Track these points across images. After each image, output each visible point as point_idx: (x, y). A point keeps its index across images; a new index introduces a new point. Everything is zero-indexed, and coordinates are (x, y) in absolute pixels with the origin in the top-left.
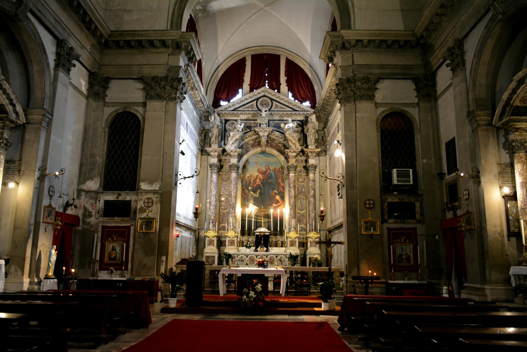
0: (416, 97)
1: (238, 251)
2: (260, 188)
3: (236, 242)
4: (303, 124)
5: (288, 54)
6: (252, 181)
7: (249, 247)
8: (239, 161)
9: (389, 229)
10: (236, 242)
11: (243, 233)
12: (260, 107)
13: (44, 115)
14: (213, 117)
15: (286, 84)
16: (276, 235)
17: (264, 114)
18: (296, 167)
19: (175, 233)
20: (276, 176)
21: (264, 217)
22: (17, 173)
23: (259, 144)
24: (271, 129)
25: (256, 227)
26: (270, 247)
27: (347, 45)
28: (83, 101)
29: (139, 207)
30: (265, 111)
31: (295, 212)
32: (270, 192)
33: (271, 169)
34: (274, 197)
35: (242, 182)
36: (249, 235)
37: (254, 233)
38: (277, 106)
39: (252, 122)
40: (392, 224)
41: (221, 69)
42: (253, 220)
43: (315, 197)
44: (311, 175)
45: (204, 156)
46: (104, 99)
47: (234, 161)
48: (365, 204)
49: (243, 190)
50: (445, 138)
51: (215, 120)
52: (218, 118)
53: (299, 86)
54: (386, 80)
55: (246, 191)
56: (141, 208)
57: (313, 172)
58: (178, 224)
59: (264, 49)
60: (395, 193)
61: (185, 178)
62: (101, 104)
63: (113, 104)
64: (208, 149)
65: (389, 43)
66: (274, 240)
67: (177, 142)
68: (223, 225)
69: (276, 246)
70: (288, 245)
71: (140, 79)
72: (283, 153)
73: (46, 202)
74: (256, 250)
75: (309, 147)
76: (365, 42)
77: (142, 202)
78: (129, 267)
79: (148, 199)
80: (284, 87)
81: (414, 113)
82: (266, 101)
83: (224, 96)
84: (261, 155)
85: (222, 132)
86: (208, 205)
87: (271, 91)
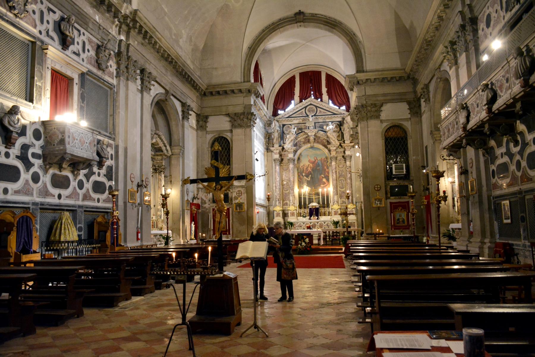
0: (409, 114)
1: (298, 220)
2: (311, 174)
3: (295, 213)
4: (340, 124)
5: (327, 70)
6: (305, 169)
7: (305, 217)
8: (294, 155)
9: (391, 203)
10: (295, 213)
11: (300, 207)
12: (308, 113)
13: (181, 150)
14: (273, 124)
15: (327, 94)
16: (324, 207)
17: (311, 119)
18: (336, 158)
19: (256, 211)
20: (322, 164)
21: (315, 195)
22: (169, 183)
23: (309, 141)
24: (316, 130)
25: (310, 203)
26: (320, 216)
27: (361, 82)
28: (195, 132)
29: (233, 196)
30: (312, 116)
31: (337, 191)
32: (319, 176)
33: (318, 159)
34: (322, 180)
35: (298, 170)
36: (305, 208)
37: (308, 207)
38: (320, 111)
39: (303, 125)
40: (393, 200)
41: (278, 85)
42: (307, 197)
43: (351, 179)
44: (348, 163)
45: (269, 153)
46: (206, 129)
47: (291, 156)
48: (375, 188)
49: (299, 176)
50: (425, 145)
51: (276, 126)
52: (277, 124)
53: (337, 94)
54: (388, 104)
55: (301, 176)
56: (235, 197)
57: (349, 160)
58: (257, 205)
59: (308, 68)
60: (395, 179)
61: (260, 176)
62: (205, 132)
63: (212, 132)
64: (272, 149)
65: (389, 79)
66: (323, 211)
67: (253, 154)
68: (285, 202)
69: (325, 215)
70: (333, 214)
71: (228, 115)
72: (326, 147)
73: (186, 199)
74: (310, 219)
75: (346, 142)
76: (373, 80)
77: (235, 193)
78: (231, 233)
79: (239, 191)
80: (325, 97)
81: (408, 125)
82: (312, 108)
83: (281, 107)
84: (311, 150)
85: (281, 136)
86: (274, 188)
87: (315, 100)
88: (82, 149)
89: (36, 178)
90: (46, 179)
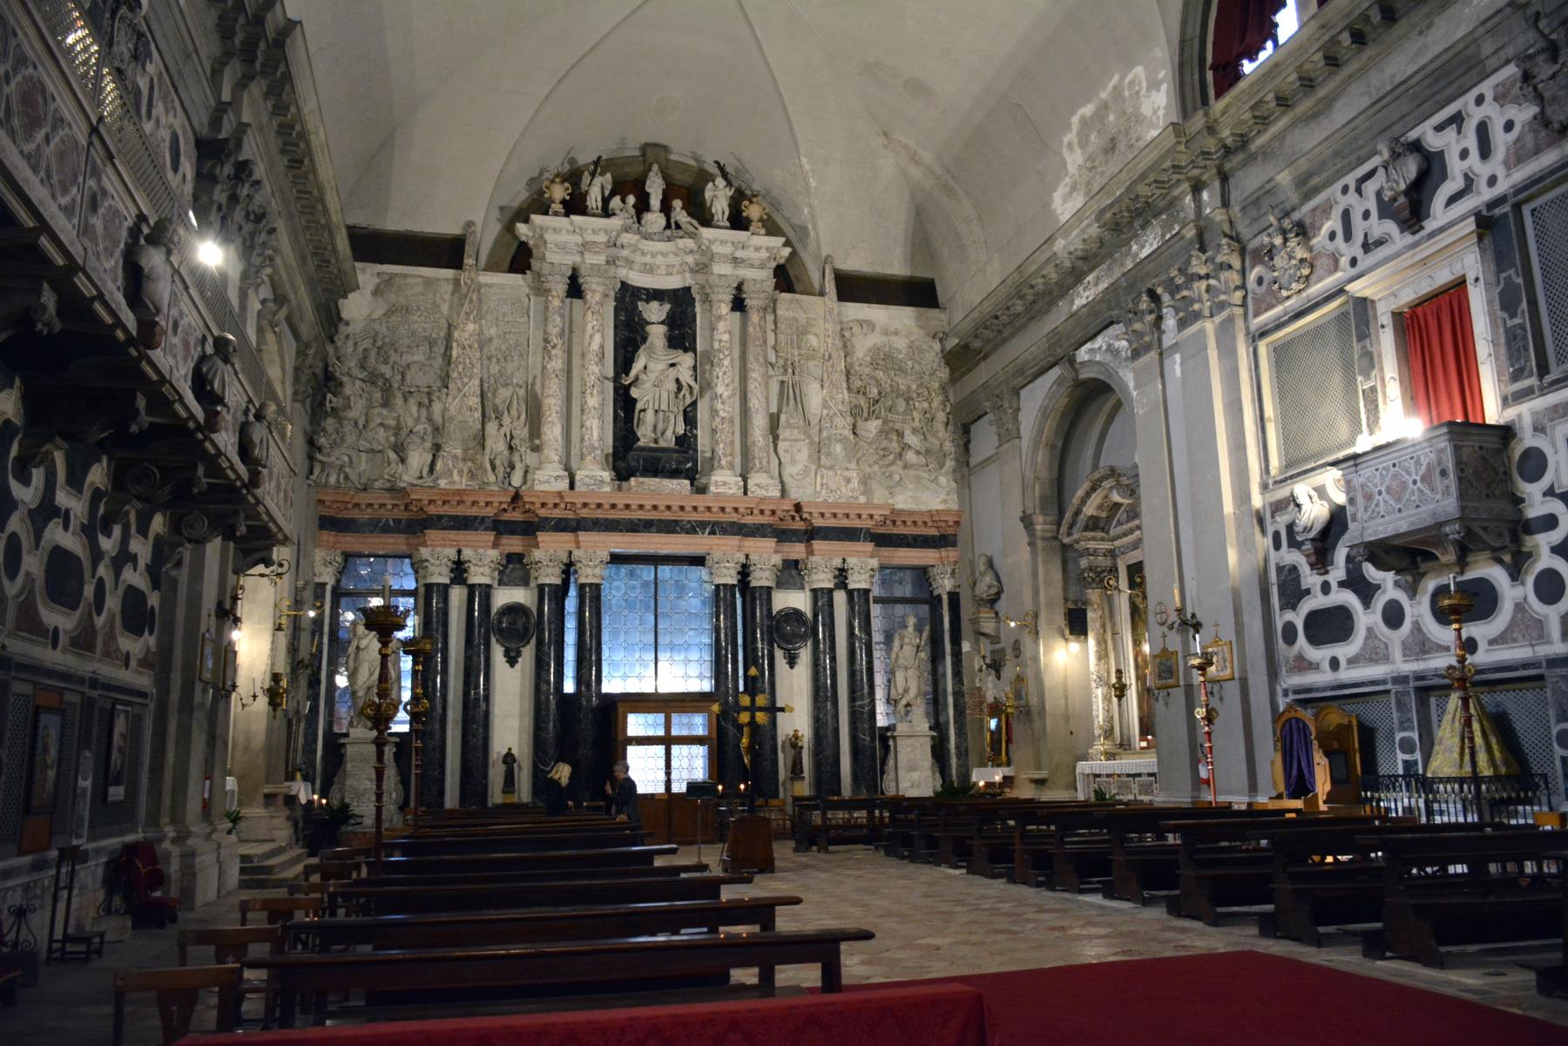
88: (1400, 510)
89: (1393, 616)
90: (1418, 610)
